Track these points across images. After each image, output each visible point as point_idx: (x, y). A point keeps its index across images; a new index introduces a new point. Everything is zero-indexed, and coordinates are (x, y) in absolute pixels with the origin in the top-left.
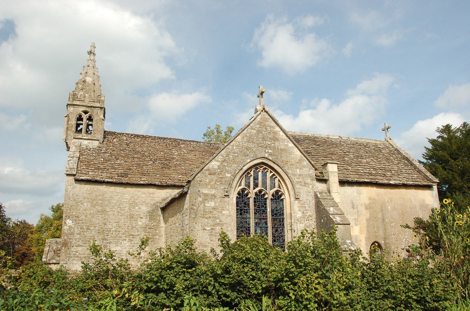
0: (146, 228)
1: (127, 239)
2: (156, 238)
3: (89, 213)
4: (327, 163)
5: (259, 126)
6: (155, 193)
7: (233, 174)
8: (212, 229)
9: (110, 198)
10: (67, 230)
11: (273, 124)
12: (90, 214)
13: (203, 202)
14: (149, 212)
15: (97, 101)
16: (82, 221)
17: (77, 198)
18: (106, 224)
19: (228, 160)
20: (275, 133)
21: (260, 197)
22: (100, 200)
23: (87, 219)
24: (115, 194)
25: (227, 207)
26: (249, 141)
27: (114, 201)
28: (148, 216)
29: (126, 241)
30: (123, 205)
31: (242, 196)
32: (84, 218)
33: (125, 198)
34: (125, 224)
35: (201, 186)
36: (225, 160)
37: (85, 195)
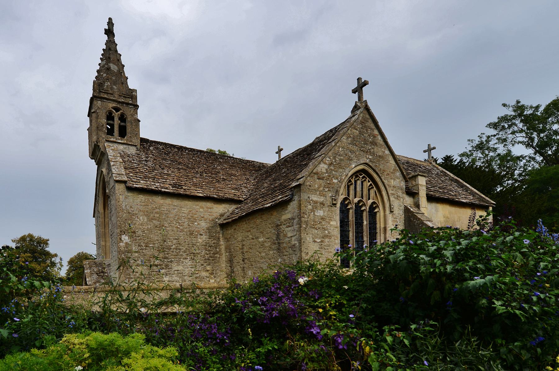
0: (206, 245)
1: (189, 258)
2: (217, 257)
3: (146, 228)
4: (419, 175)
5: (361, 126)
6: (213, 208)
7: (339, 180)
8: (322, 241)
9: (167, 212)
10: (124, 247)
11: (372, 126)
12: (148, 230)
13: (313, 210)
14: (208, 229)
15: (128, 96)
16: (139, 238)
17: (132, 210)
18: (165, 241)
19: (335, 163)
20: (375, 137)
21: (358, 206)
22: (157, 213)
23: (144, 235)
24: (173, 207)
25: (335, 218)
26: (352, 143)
27: (172, 215)
28: (207, 233)
29: (188, 260)
30: (181, 220)
31: (344, 211)
32: (141, 234)
33: (182, 211)
34: (185, 241)
35: (311, 192)
36: (332, 163)
37: (142, 208)
